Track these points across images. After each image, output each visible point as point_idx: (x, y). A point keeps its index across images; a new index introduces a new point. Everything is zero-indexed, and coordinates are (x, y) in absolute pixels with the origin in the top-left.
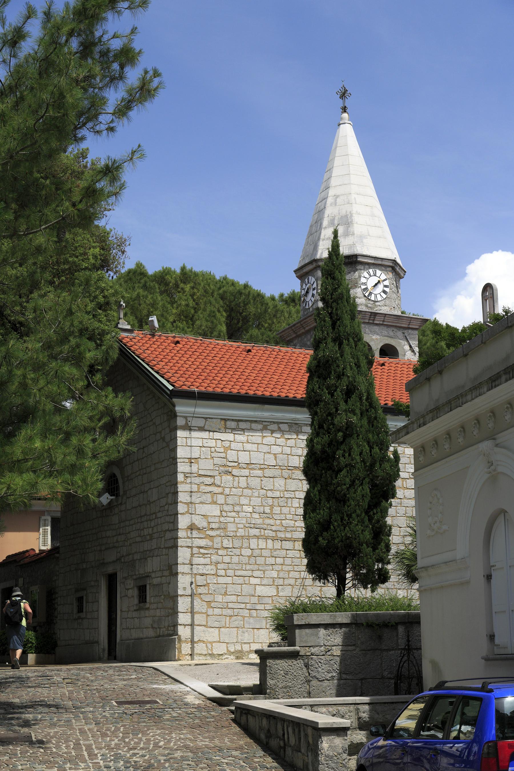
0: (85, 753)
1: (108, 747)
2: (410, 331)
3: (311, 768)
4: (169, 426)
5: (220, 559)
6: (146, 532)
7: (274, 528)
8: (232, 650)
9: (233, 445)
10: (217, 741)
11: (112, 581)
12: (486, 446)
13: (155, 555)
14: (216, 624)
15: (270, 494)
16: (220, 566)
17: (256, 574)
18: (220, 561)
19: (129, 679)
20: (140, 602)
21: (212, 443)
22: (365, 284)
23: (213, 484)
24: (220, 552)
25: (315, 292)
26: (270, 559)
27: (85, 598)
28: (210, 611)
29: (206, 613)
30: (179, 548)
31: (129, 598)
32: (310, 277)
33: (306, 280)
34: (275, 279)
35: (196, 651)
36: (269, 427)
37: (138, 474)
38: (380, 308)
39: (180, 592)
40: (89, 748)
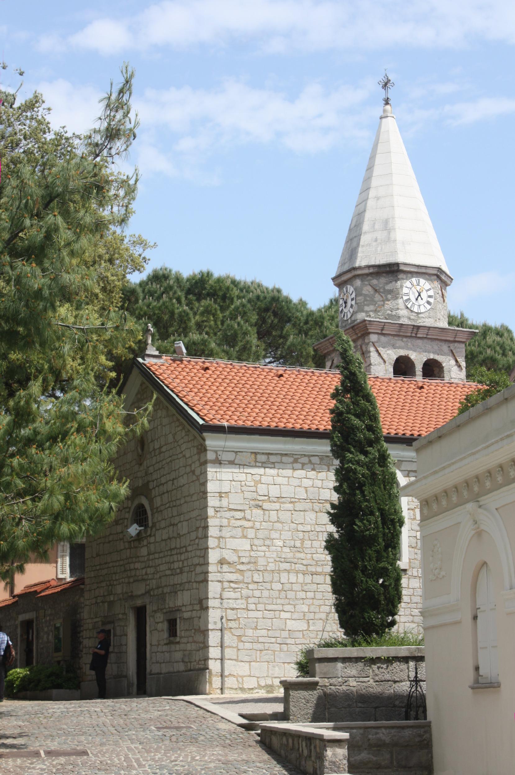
0: (135, 764)
1: (153, 759)
2: (456, 344)
3: (318, 772)
4: (199, 460)
5: (250, 593)
6: (176, 565)
7: (305, 562)
8: (263, 684)
9: (264, 479)
10: (244, 757)
11: (141, 614)
12: (470, 506)
13: (186, 588)
14: (247, 658)
15: (300, 528)
16: (250, 601)
17: (287, 608)
18: (251, 595)
19: (163, 710)
20: (170, 636)
21: (242, 477)
22: (407, 294)
23: (244, 518)
24: (251, 586)
25: (353, 302)
26: (300, 593)
27: (112, 631)
28: (241, 645)
29: (237, 647)
30: (210, 583)
31: (159, 631)
32: (349, 286)
33: (345, 289)
34: (311, 289)
35: (227, 685)
36: (299, 460)
37: (168, 505)
38: (424, 320)
39: (211, 626)
40: (137, 760)
